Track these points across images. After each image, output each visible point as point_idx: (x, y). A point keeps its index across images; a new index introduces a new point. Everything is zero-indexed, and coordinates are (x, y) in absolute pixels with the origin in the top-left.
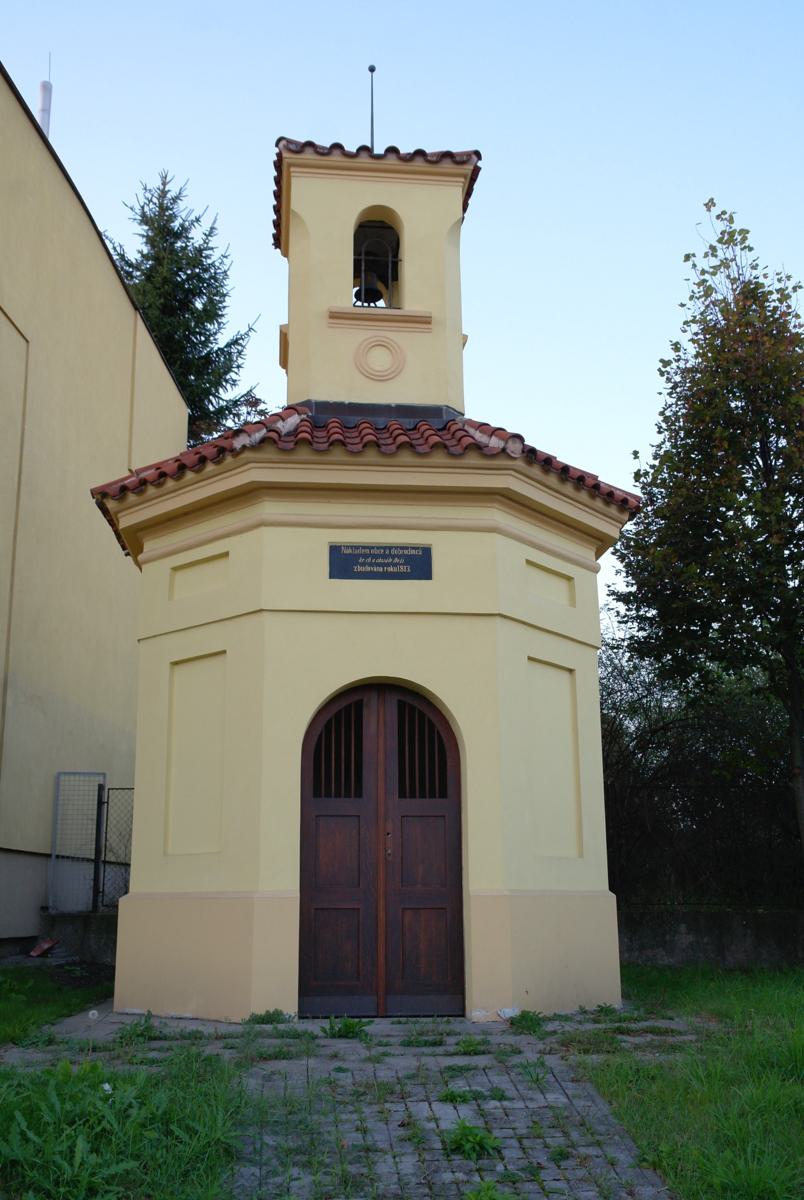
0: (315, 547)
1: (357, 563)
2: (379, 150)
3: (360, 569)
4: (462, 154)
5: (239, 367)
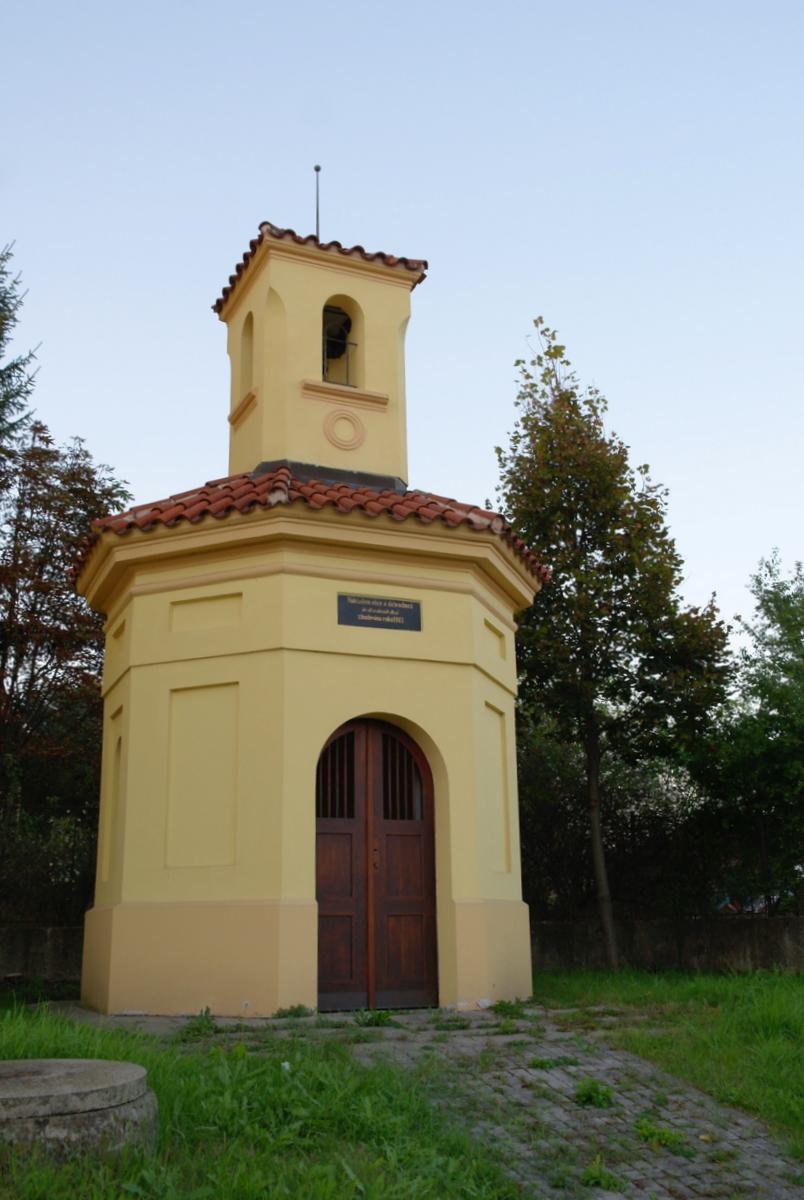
0: (323, 597)
1: (360, 613)
2: (324, 240)
3: (362, 617)
4: (414, 261)
5: (28, 392)
